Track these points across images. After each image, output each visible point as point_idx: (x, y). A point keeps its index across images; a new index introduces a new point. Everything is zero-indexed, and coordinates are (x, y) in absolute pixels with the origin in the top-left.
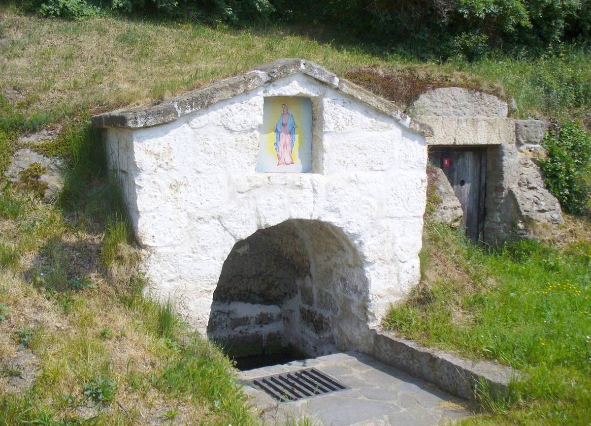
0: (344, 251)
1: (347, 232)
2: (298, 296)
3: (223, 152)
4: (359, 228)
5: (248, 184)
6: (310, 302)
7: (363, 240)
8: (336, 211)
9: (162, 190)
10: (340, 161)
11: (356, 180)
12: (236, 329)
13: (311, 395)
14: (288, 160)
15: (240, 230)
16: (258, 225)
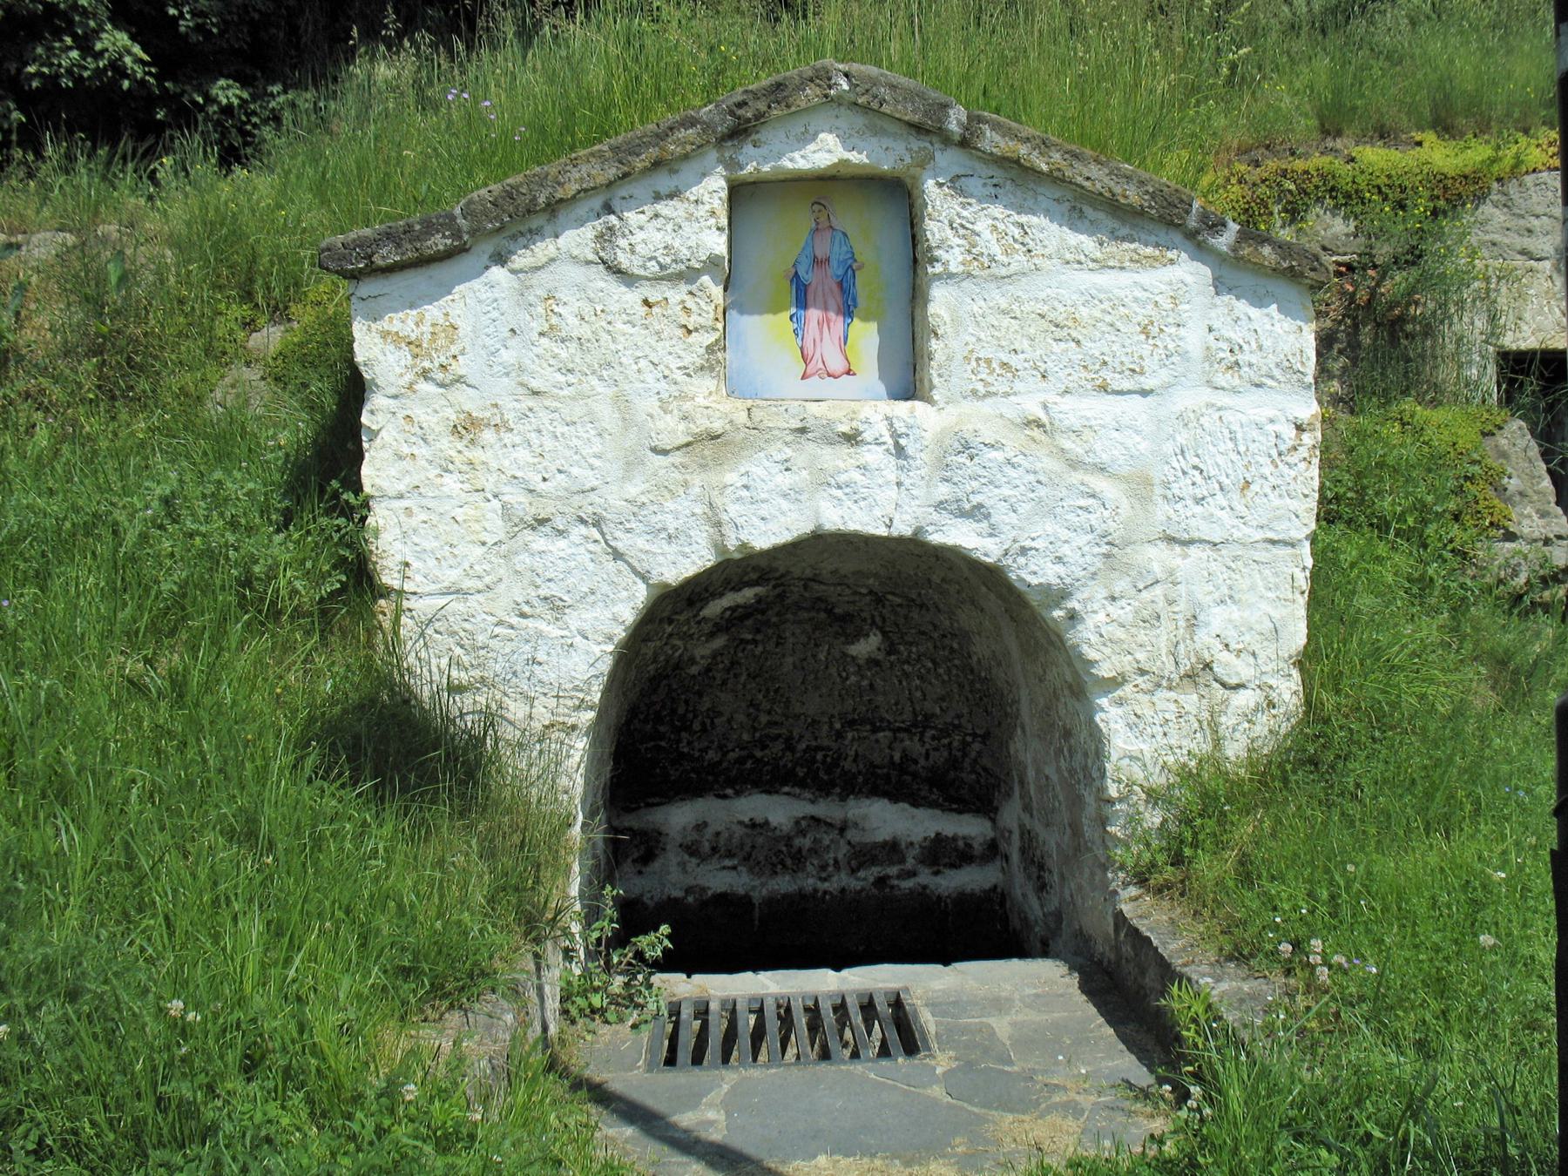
1: (1022, 580)
3: (604, 337)
4: (1060, 569)
5: (682, 426)
7: (1077, 606)
8: (976, 513)
9: (430, 438)
10: (988, 361)
11: (1045, 419)
12: (861, 874)
14: (836, 364)
16: (716, 546)
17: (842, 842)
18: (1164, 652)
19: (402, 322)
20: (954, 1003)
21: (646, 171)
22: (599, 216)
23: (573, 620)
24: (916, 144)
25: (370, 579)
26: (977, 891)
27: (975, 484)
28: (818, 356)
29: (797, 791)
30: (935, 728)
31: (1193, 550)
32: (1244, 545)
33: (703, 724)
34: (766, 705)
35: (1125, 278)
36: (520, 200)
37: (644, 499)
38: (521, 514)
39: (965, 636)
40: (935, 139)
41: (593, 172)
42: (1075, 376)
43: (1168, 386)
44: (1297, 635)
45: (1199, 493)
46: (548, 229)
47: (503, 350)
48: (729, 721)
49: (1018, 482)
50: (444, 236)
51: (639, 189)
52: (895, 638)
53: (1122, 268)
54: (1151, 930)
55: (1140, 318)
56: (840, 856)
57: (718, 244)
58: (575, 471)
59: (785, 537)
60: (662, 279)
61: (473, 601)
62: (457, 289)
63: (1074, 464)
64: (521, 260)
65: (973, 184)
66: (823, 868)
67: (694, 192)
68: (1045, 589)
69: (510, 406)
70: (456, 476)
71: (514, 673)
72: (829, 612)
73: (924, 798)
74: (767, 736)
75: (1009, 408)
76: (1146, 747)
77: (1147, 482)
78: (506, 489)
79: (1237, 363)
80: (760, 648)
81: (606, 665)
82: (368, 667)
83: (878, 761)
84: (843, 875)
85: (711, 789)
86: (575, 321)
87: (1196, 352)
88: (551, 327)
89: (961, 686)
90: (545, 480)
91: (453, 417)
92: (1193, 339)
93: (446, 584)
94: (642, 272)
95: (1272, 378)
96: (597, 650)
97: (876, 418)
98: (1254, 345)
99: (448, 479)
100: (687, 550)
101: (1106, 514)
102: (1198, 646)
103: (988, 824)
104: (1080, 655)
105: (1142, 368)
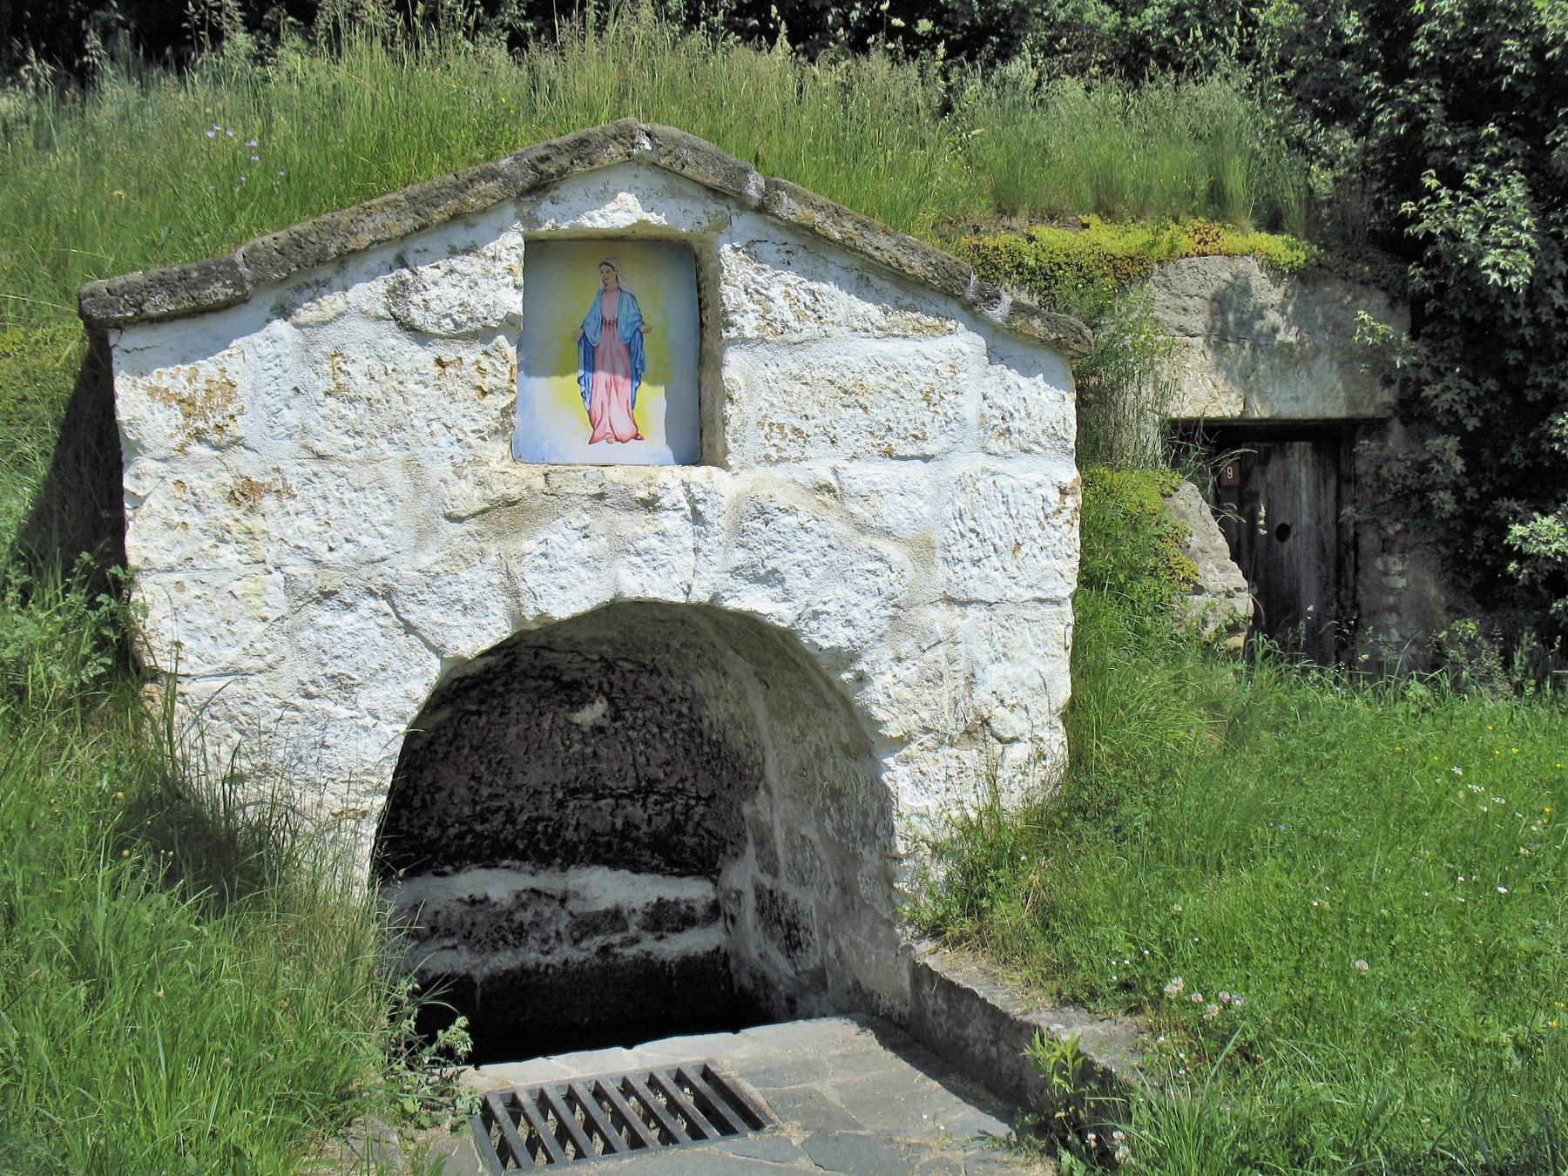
0: (827, 706)
3: (395, 397)
4: (850, 632)
5: (477, 493)
6: (771, 868)
7: (866, 668)
8: (771, 578)
9: (204, 505)
10: (781, 427)
11: (835, 485)
12: (584, 944)
13: (705, 1137)
14: (624, 428)
15: (456, 631)
16: (513, 617)
17: (564, 913)
18: (946, 709)
20: (767, 1071)
21: (445, 223)
22: (391, 270)
23: (364, 699)
24: (713, 207)
25: (137, 661)
26: (700, 953)
27: (769, 549)
28: (605, 419)
29: (517, 863)
30: (658, 793)
31: (970, 610)
32: (1016, 604)
33: (423, 800)
34: (487, 778)
35: (908, 347)
36: (309, 249)
37: (437, 569)
38: (306, 586)
39: (695, 700)
40: (732, 203)
41: (389, 222)
42: (862, 443)
44: (1063, 690)
45: (976, 554)
46: (336, 281)
47: (285, 410)
48: (450, 796)
49: (811, 547)
50: (225, 285)
51: (433, 242)
52: (621, 704)
53: (905, 337)
54: (967, 981)
55: (922, 386)
56: (562, 929)
57: (513, 302)
58: (364, 540)
59: (584, 607)
60: (456, 337)
61: (253, 683)
62: (235, 343)
63: (862, 529)
64: (306, 313)
65: (767, 250)
66: (545, 941)
67: (490, 248)
68: (836, 652)
69: (293, 471)
71: (300, 759)
72: (556, 680)
73: (645, 864)
74: (488, 809)
75: (800, 473)
76: (931, 803)
77: (929, 545)
78: (289, 560)
79: (1008, 430)
80: (484, 719)
81: (397, 748)
82: (138, 759)
83: (600, 829)
84: (565, 947)
85: (430, 867)
87: (972, 418)
88: (339, 386)
89: (687, 751)
90: (331, 549)
91: (231, 482)
92: (970, 407)
93: (223, 665)
94: (437, 331)
95: (1039, 444)
96: (388, 729)
97: (674, 484)
98: (1023, 413)
99: (224, 550)
100: (483, 621)
101: (893, 577)
103: (710, 886)
104: (870, 716)
105: (924, 434)
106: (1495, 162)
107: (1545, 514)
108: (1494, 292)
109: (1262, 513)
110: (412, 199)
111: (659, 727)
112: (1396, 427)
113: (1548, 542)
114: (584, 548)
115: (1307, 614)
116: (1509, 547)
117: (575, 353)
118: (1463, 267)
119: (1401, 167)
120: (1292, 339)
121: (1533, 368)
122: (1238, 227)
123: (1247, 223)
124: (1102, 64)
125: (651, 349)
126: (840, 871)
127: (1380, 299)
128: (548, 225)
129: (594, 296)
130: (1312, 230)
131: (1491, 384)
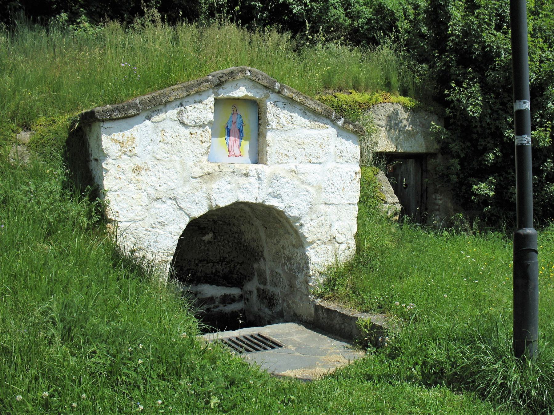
0: (289, 233)
1: (289, 215)
2: (256, 278)
3: (179, 143)
4: (299, 212)
5: (200, 171)
7: (303, 222)
8: (278, 196)
9: (125, 173)
10: (282, 154)
11: (296, 170)
14: (237, 153)
15: (194, 210)
19: (118, 136)
23: (167, 228)
27: (278, 188)
31: (331, 206)
35: (316, 132)
37: (189, 192)
39: (242, 233)
43: (326, 162)
44: (355, 230)
45: (333, 191)
46: (164, 110)
51: (190, 99)
52: (217, 234)
57: (211, 117)
58: (169, 183)
59: (228, 203)
61: (138, 223)
62: (135, 126)
63: (303, 183)
65: (279, 104)
67: (205, 102)
68: (295, 217)
70: (133, 185)
72: (199, 227)
76: (319, 261)
78: (149, 189)
81: (176, 243)
83: (208, 273)
86: (170, 138)
87: (333, 153)
88: (163, 140)
89: (236, 248)
91: (133, 166)
92: (332, 149)
94: (190, 124)
102: (332, 232)
103: (240, 290)
104: (304, 236)
106: (471, 79)
107: (483, 182)
108: (470, 118)
109: (405, 181)
110: (185, 87)
111: (228, 241)
112: (440, 156)
113: (483, 191)
114: (229, 187)
115: (416, 209)
116: (473, 192)
117: (225, 131)
118: (461, 110)
119: (443, 79)
120: (410, 129)
121: (480, 140)
122: (395, 94)
123: (398, 93)
124: (345, 36)
125: (245, 131)
126: (290, 281)
127: (436, 117)
128: (221, 95)
129: (230, 115)
130: (416, 97)
131: (468, 144)
